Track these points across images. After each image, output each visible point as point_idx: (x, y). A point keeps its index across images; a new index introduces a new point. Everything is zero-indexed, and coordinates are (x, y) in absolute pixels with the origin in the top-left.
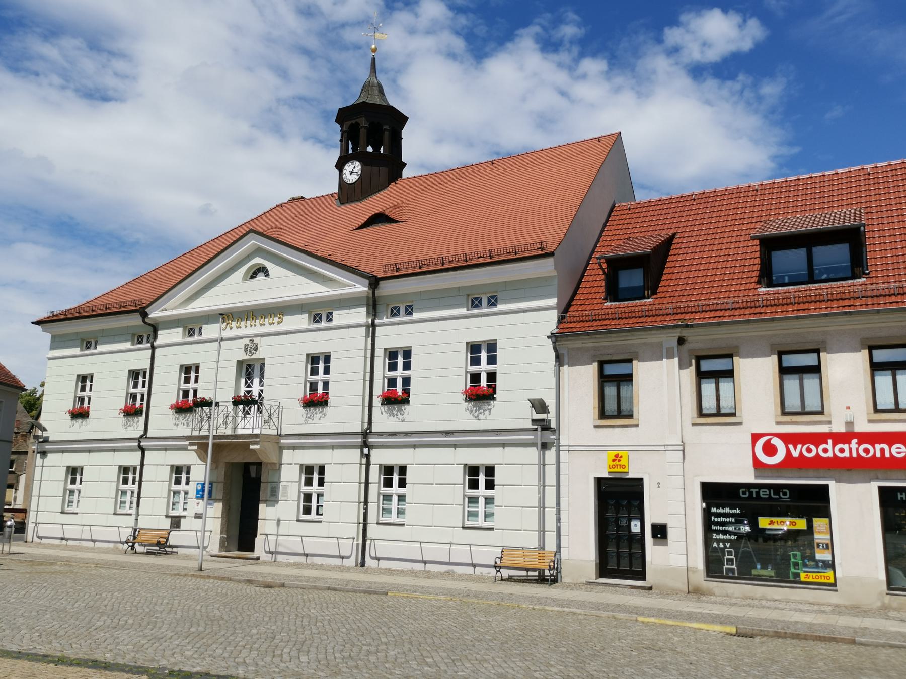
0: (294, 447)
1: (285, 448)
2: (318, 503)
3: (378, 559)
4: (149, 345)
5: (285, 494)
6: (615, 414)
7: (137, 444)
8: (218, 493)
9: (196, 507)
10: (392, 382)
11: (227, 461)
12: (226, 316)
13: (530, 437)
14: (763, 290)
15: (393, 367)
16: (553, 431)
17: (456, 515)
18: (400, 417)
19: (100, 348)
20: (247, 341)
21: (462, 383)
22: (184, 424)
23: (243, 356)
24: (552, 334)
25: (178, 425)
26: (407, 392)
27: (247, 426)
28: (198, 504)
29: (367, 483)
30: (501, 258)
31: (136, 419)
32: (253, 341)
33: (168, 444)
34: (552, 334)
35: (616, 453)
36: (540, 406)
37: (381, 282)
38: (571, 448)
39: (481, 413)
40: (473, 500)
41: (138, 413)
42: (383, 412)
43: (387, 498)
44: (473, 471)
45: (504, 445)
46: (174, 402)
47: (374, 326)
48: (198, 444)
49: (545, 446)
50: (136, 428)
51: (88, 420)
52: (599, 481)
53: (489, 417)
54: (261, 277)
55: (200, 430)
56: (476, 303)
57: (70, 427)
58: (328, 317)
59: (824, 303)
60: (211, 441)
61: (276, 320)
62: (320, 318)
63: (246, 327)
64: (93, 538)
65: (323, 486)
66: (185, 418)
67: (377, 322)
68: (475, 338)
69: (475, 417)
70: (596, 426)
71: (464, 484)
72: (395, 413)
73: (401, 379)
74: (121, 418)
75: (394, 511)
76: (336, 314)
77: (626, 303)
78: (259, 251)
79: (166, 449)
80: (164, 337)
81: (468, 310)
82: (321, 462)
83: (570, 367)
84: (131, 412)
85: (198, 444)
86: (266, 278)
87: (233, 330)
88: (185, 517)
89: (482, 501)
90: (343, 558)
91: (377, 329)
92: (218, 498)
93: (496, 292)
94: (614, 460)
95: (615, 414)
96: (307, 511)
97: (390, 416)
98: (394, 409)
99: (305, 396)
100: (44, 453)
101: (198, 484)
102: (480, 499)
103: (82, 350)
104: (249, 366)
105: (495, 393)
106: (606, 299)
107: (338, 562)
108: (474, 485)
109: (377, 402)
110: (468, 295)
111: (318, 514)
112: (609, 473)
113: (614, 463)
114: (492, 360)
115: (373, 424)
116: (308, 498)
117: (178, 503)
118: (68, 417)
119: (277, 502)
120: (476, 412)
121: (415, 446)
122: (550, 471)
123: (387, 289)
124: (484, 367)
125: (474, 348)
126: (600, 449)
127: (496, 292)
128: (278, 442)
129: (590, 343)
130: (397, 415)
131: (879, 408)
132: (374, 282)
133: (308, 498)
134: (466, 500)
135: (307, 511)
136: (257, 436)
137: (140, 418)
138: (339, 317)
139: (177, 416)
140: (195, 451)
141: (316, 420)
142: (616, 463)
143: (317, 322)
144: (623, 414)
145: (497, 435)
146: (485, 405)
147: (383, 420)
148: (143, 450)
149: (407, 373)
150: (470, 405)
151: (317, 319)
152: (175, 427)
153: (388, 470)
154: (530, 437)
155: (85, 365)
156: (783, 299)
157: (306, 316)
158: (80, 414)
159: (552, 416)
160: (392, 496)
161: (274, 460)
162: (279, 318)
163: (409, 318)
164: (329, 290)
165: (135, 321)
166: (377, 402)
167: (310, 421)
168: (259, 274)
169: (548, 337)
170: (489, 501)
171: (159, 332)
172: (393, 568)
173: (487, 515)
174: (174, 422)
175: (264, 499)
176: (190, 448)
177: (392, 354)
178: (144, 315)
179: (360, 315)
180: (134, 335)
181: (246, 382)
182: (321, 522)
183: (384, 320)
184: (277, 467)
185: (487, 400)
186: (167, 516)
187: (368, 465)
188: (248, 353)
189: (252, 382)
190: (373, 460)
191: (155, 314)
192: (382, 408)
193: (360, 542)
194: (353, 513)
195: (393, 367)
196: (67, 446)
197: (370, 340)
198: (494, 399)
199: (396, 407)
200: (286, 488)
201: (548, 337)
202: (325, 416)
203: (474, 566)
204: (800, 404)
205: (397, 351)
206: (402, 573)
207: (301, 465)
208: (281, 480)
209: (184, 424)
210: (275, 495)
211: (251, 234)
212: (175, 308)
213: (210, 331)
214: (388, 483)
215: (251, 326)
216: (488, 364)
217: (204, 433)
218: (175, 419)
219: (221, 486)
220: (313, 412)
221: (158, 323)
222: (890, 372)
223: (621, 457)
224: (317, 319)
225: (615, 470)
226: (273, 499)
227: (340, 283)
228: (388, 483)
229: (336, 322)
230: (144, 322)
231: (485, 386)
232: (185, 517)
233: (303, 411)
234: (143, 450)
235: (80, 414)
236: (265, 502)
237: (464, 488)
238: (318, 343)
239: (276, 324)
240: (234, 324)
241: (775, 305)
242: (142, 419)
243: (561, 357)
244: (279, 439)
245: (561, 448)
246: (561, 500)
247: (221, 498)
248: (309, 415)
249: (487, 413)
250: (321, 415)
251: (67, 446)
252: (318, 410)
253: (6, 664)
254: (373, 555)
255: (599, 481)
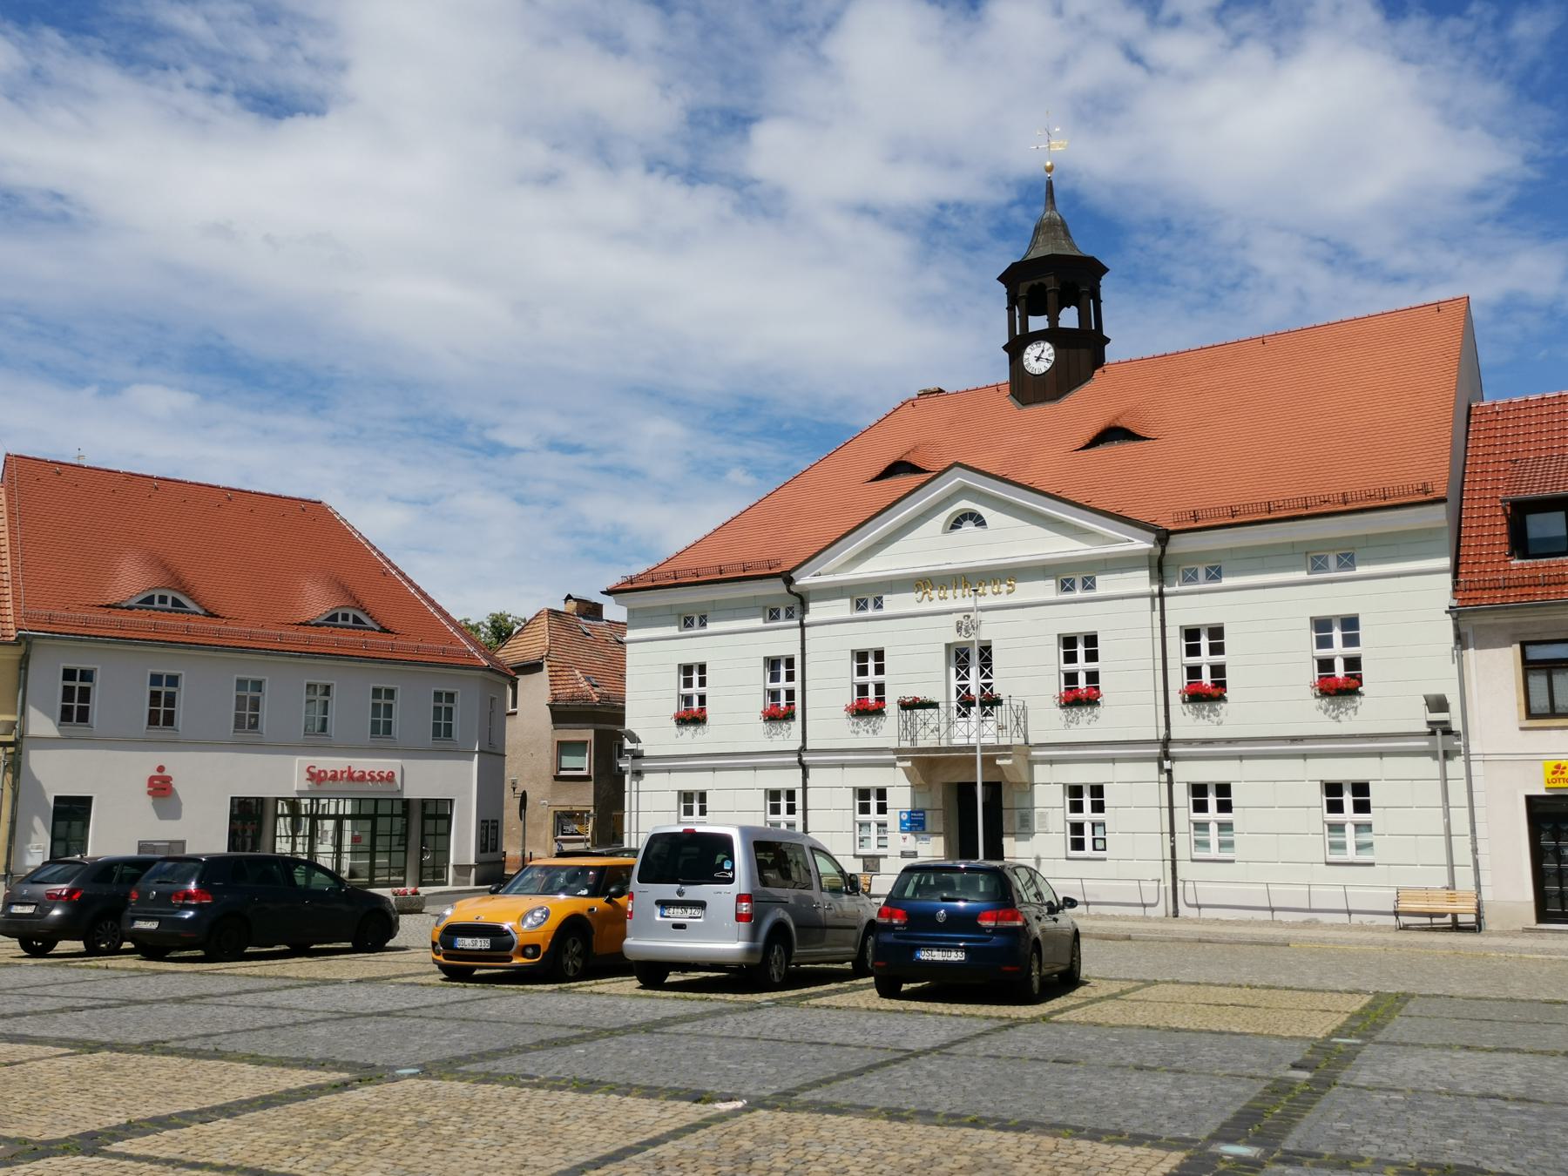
0: (1051, 761)
1: (1036, 762)
2: (1093, 834)
3: (1199, 907)
4: (798, 622)
5: (1043, 824)
6: (1548, 711)
7: (796, 759)
8: (934, 820)
9: (902, 843)
10: (1194, 672)
11: (945, 781)
12: (922, 583)
13: (1423, 744)
14: (1516, 562)
15: (1193, 651)
16: (1458, 735)
17: (1317, 845)
18: (1216, 719)
19: (1361, 570)
20: (959, 617)
21: (759, 703)
22: (868, 732)
23: (954, 638)
24: (1450, 607)
25: (858, 733)
26: (1221, 685)
27: (973, 732)
28: (905, 839)
29: (1171, 807)
30: (1396, 501)
31: (785, 725)
32: (969, 617)
33: (841, 758)
34: (1450, 607)
35: (1558, 762)
36: (1438, 704)
37: (1171, 537)
38: (1487, 758)
39: (1342, 713)
40: (1337, 828)
41: (789, 716)
42: (1187, 712)
43: (1201, 827)
44: (863, 794)
45: (1381, 754)
46: (849, 704)
47: (1161, 595)
48: (913, 760)
49: (1447, 755)
50: (788, 736)
51: (706, 727)
52: (1530, 800)
53: (1354, 718)
54: (969, 527)
55: (968, 737)
56: (688, 623)
57: (677, 737)
58: (876, 603)
59: (1540, 588)
60: (979, 754)
61: (1004, 588)
62: (866, 604)
63: (955, 598)
64: (1199, 903)
65: (1103, 812)
66: (869, 723)
67: (1166, 590)
68: (1070, 629)
69: (1333, 718)
70: (1522, 729)
71: (854, 809)
72: (1206, 713)
73: (1209, 668)
74: (762, 726)
75: (1351, 846)
76: (1099, 579)
77: (1545, 560)
78: (964, 492)
79: (843, 766)
80: (817, 611)
81: (765, 622)
82: (701, 788)
83: (1478, 651)
84: (777, 715)
85: (913, 760)
86: (979, 529)
87: (936, 601)
88: (886, 856)
89: (1213, 828)
90: (1145, 906)
91: (1166, 599)
92: (936, 831)
93: (1353, 548)
94: (1554, 773)
95: (1548, 711)
96: (1078, 845)
97: (1198, 717)
98: (1204, 709)
99: (853, 704)
100: (638, 774)
101: (901, 813)
102: (1211, 825)
103: (680, 630)
104: (962, 650)
105: (1361, 685)
106: (1511, 554)
107: (1139, 911)
108: (865, 809)
109: (1175, 698)
110: (1307, 553)
111: (1095, 849)
112: (1547, 788)
113: (1554, 776)
114: (1092, 656)
115: (1172, 729)
116: (1077, 828)
117: (869, 838)
118: (673, 723)
119: (1033, 834)
120: (1333, 711)
121: (1241, 757)
122: (1458, 790)
123: (1178, 545)
124: (1081, 666)
125: (1322, 626)
126: (1532, 758)
127: (1353, 548)
128: (1027, 753)
129: (1506, 619)
130: (1208, 716)
131: (1533, 712)
132: (1163, 537)
133: (1077, 828)
134: (1192, 825)
135: (1078, 845)
136: (1008, 748)
137: (792, 723)
138: (1106, 584)
139: (856, 721)
140: (905, 769)
141: (1083, 724)
142: (1559, 775)
143: (1068, 590)
144: (1558, 711)
145: (1371, 742)
146: (1347, 702)
147: (1187, 723)
148: (805, 768)
149: (880, 678)
150: (1325, 702)
151: (860, 605)
152: (855, 735)
153: (1199, 790)
154: (1423, 744)
155: (692, 648)
156: (1530, 577)
157: (848, 601)
158: (692, 717)
159: (1454, 718)
160: (1344, 825)
161: (1025, 779)
162: (1009, 585)
163: (702, 631)
164: (1089, 547)
165: (777, 588)
166: (1175, 698)
167: (1073, 725)
168: (965, 523)
169: (1447, 612)
170: (1225, 827)
171: (811, 605)
172: (1224, 918)
173: (1222, 845)
174: (851, 728)
175: (1010, 831)
176: (898, 764)
177: (1192, 634)
178: (788, 579)
179: (1141, 581)
180: (765, 608)
181: (958, 673)
182: (1105, 859)
183: (1177, 588)
184: (1028, 788)
185: (1350, 694)
186: (855, 856)
187: (1170, 782)
188: (963, 633)
189: (968, 673)
190: (1176, 776)
191: (804, 580)
192: (1185, 707)
193: (1169, 884)
194: (1157, 847)
195: (1193, 651)
196: (673, 764)
197: (1157, 614)
198: (1360, 694)
199: (1207, 706)
200: (1043, 815)
201: (1447, 612)
202: (1097, 718)
203: (1349, 912)
204: (1548, 704)
205: (1075, 638)
206: (1248, 923)
207: (854, 788)
208: (1036, 805)
209: (868, 732)
210: (1027, 826)
211: (955, 469)
212: (833, 572)
213: (893, 603)
214: (1200, 807)
215: (964, 596)
216: (1087, 661)
217: (973, 741)
218: (853, 724)
219: (939, 814)
220: (1076, 714)
221: (808, 592)
222: (1545, 672)
223: (1565, 768)
224: (860, 605)
225: (1557, 785)
226: (1025, 829)
227: (1103, 537)
228: (1200, 807)
229: (887, 610)
230: (790, 592)
231: (1209, 684)
232: (886, 856)
233: (1061, 712)
234: (805, 768)
235: (692, 717)
236: (1012, 834)
237: (854, 813)
238: (1078, 620)
239: (1004, 593)
240: (934, 594)
241: (1560, 583)
242: (796, 725)
243: (1463, 637)
244: (1028, 751)
245: (1472, 758)
246: (1477, 825)
247: (941, 830)
248: (1070, 718)
249: (1351, 712)
250: (1090, 717)
251: (673, 764)
252: (1086, 711)
253: (3, 971)
254: (1192, 901)
255: (1530, 800)
